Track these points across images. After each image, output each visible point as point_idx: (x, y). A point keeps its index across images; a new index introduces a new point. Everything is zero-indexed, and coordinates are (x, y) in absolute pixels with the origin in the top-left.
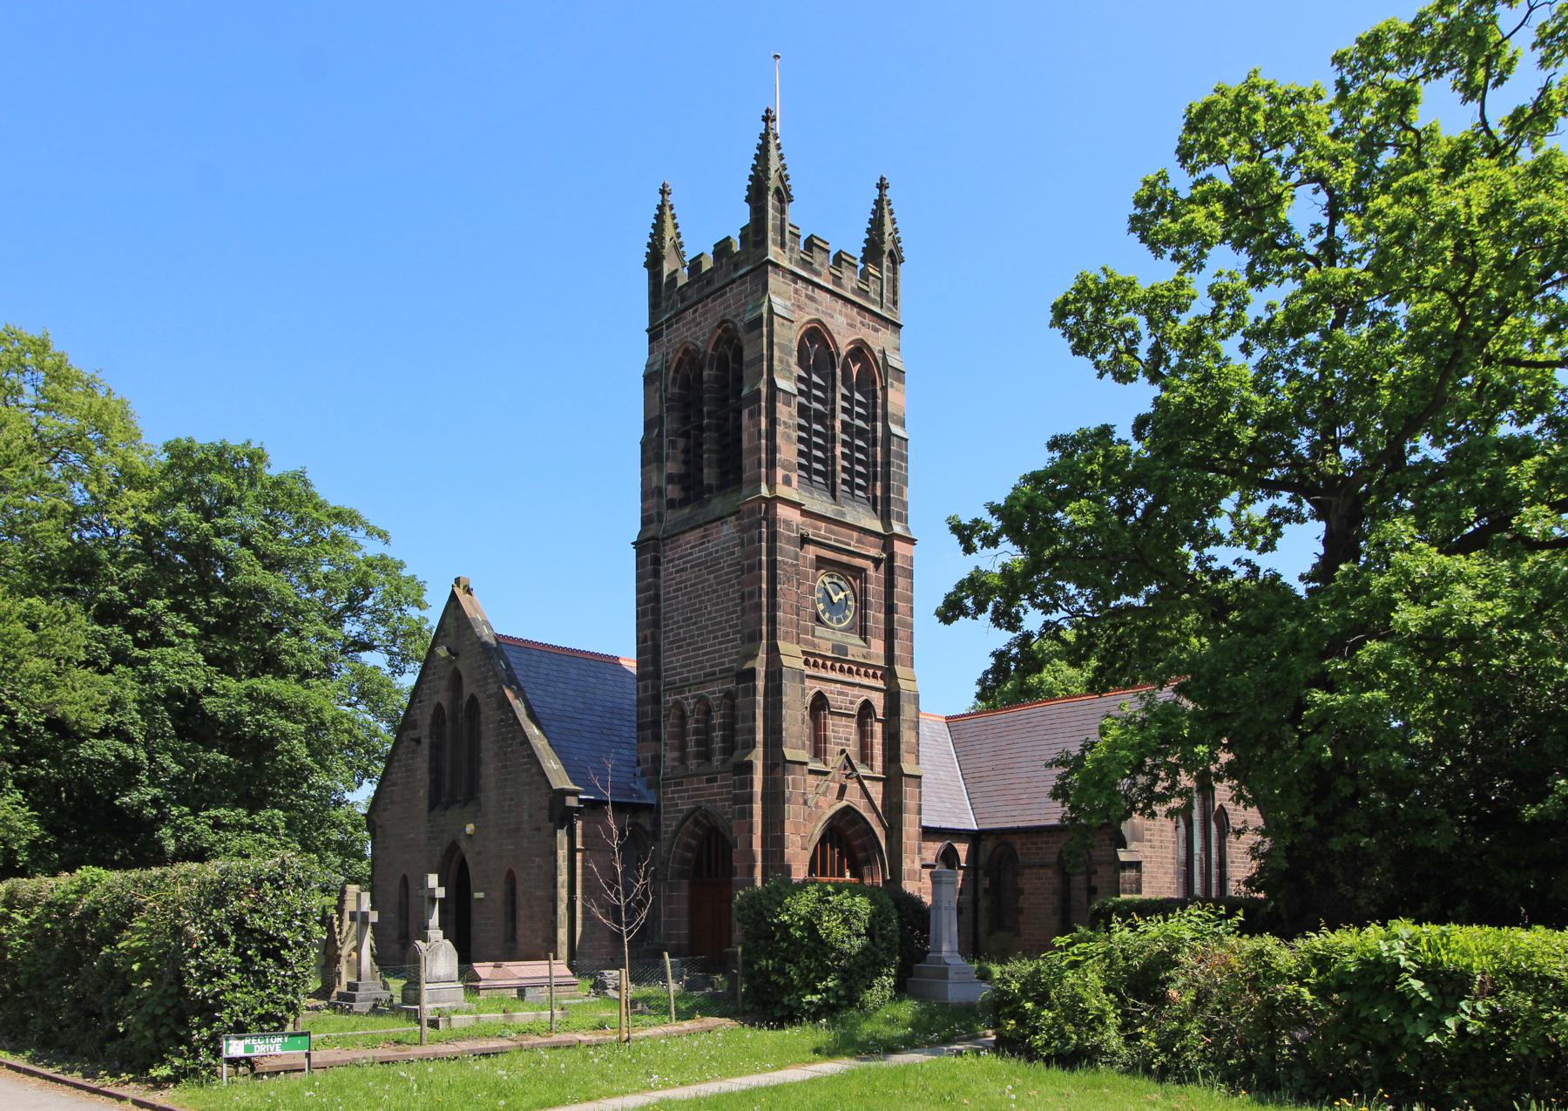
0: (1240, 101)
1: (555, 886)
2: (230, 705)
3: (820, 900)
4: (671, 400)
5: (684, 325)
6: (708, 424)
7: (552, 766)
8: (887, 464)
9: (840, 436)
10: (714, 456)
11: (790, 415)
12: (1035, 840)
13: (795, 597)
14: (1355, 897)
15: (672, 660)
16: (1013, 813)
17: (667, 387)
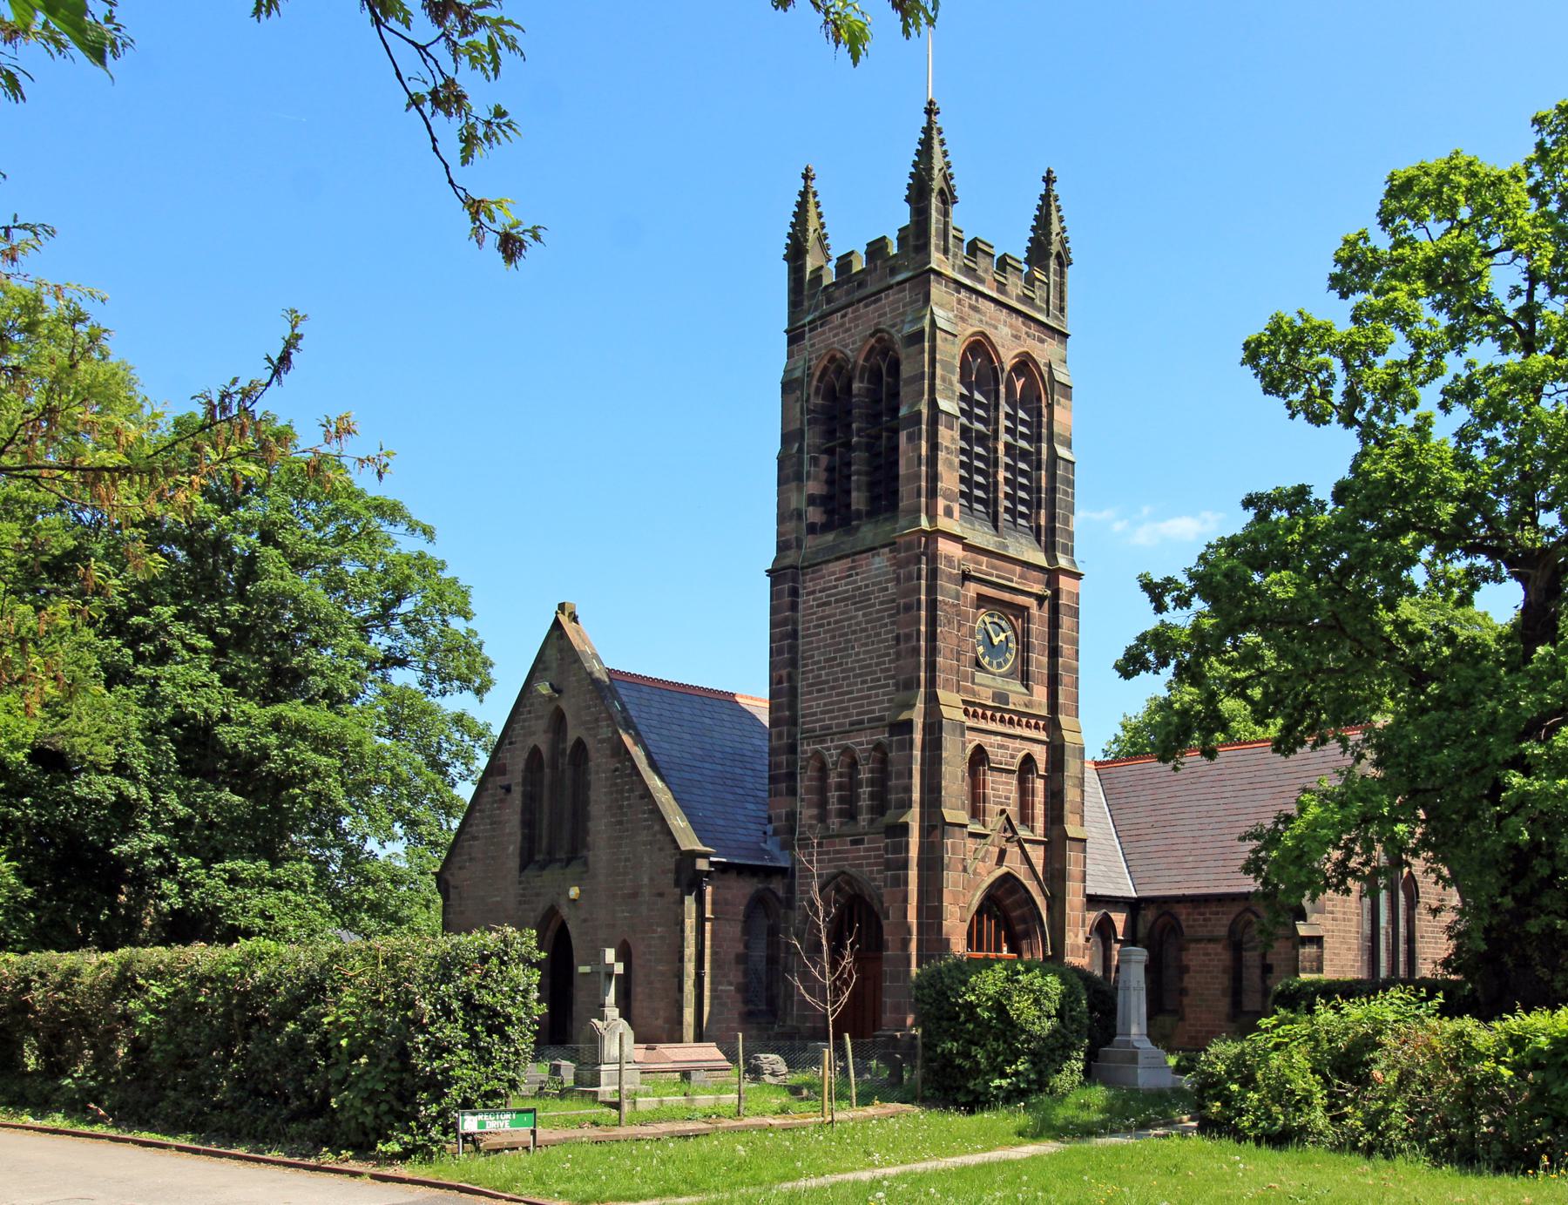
0: (1443, 178)
1: (681, 960)
2: (253, 735)
3: (1008, 979)
4: (813, 411)
5: (831, 330)
6: (858, 443)
7: (679, 823)
8: (1052, 490)
9: (1003, 459)
10: (864, 478)
11: (953, 439)
12: (1202, 910)
13: (955, 641)
14: (1552, 980)
15: (811, 705)
16: (1178, 878)
17: (809, 395)
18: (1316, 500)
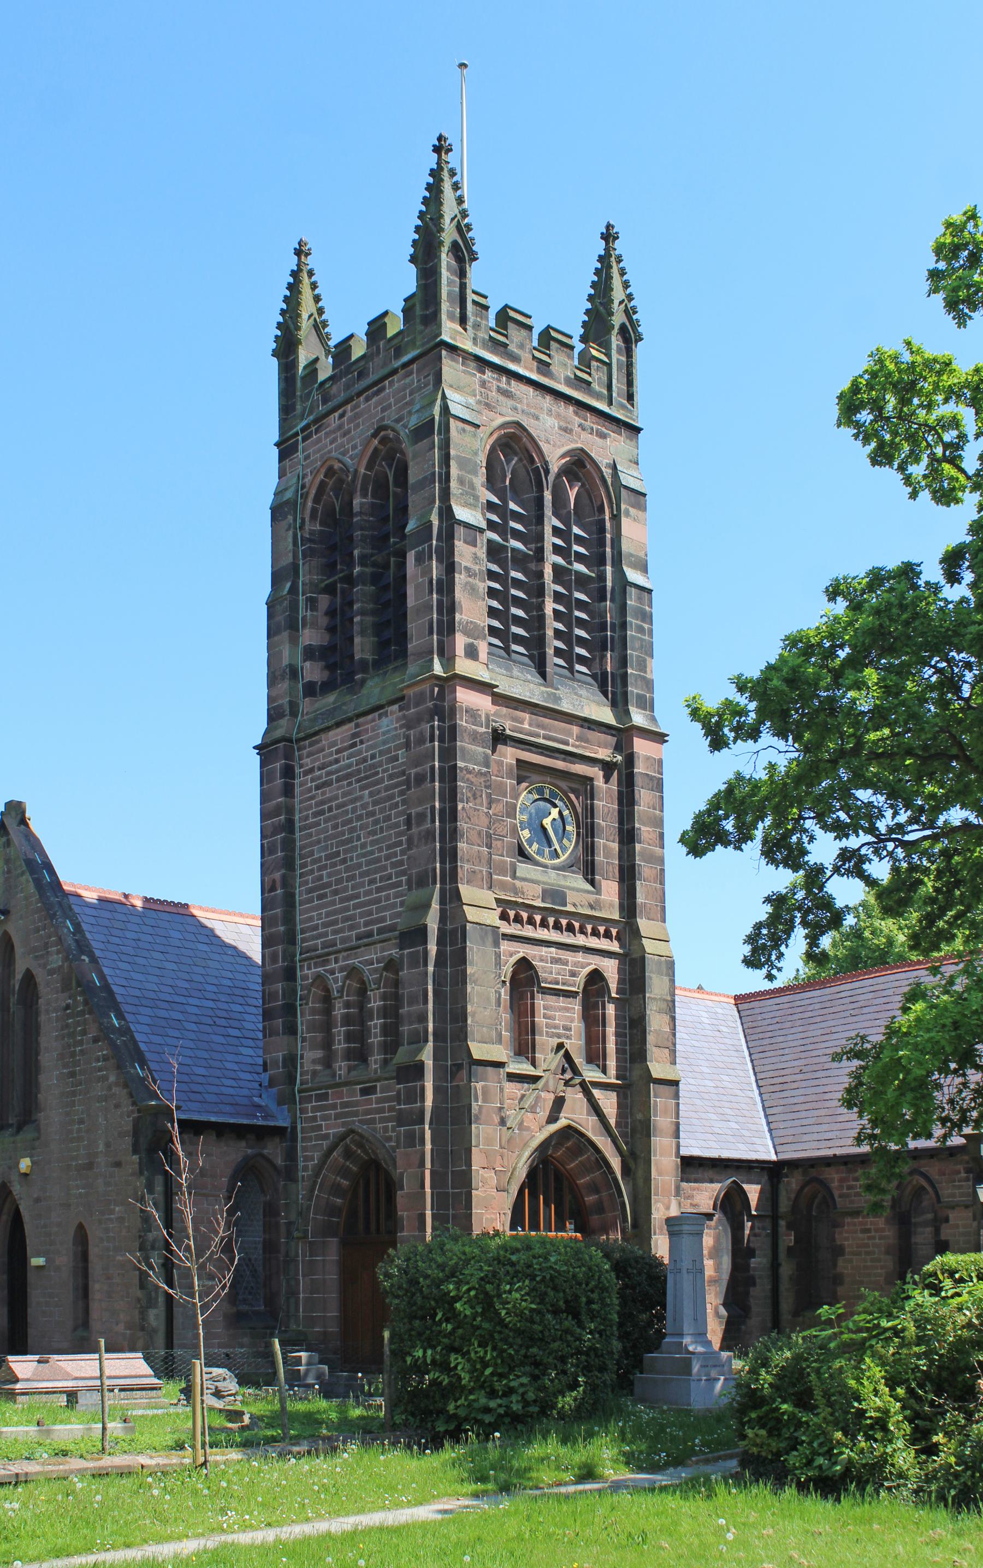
4: (310, 540)
5: (327, 435)
6: (361, 574)
10: (369, 619)
11: (476, 558)
13: (485, 821)
18: (927, 583)
